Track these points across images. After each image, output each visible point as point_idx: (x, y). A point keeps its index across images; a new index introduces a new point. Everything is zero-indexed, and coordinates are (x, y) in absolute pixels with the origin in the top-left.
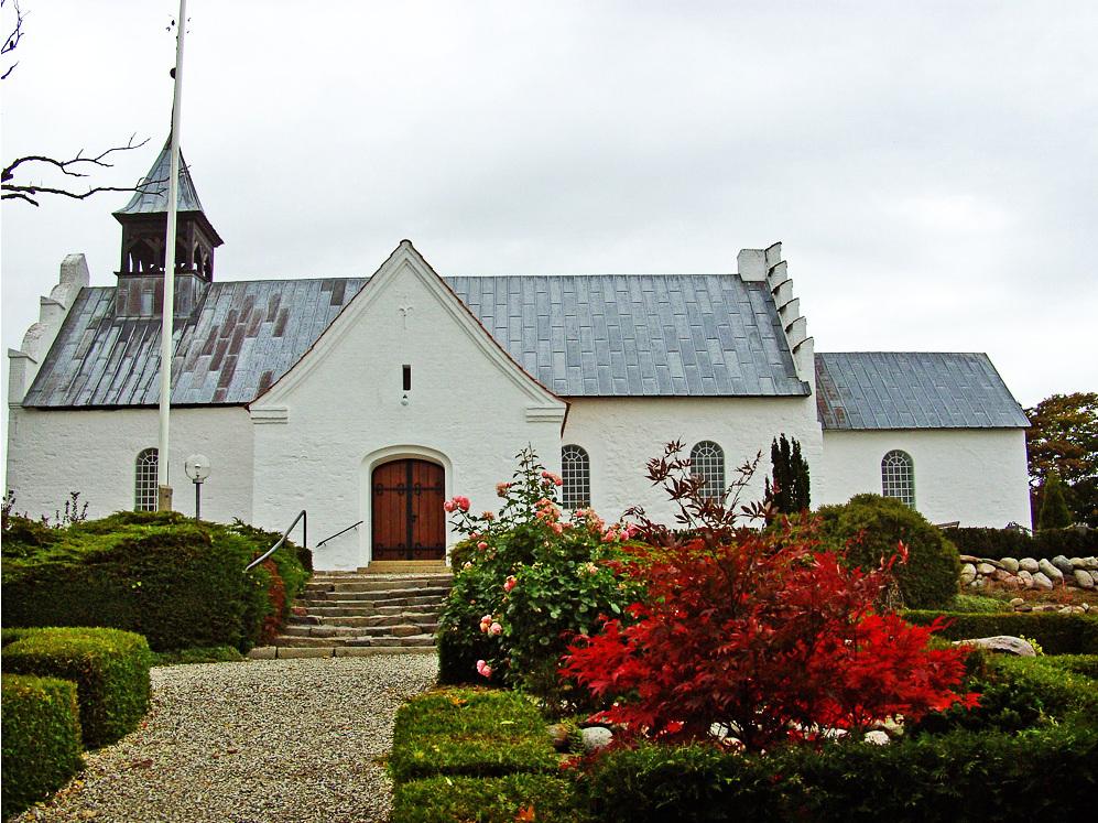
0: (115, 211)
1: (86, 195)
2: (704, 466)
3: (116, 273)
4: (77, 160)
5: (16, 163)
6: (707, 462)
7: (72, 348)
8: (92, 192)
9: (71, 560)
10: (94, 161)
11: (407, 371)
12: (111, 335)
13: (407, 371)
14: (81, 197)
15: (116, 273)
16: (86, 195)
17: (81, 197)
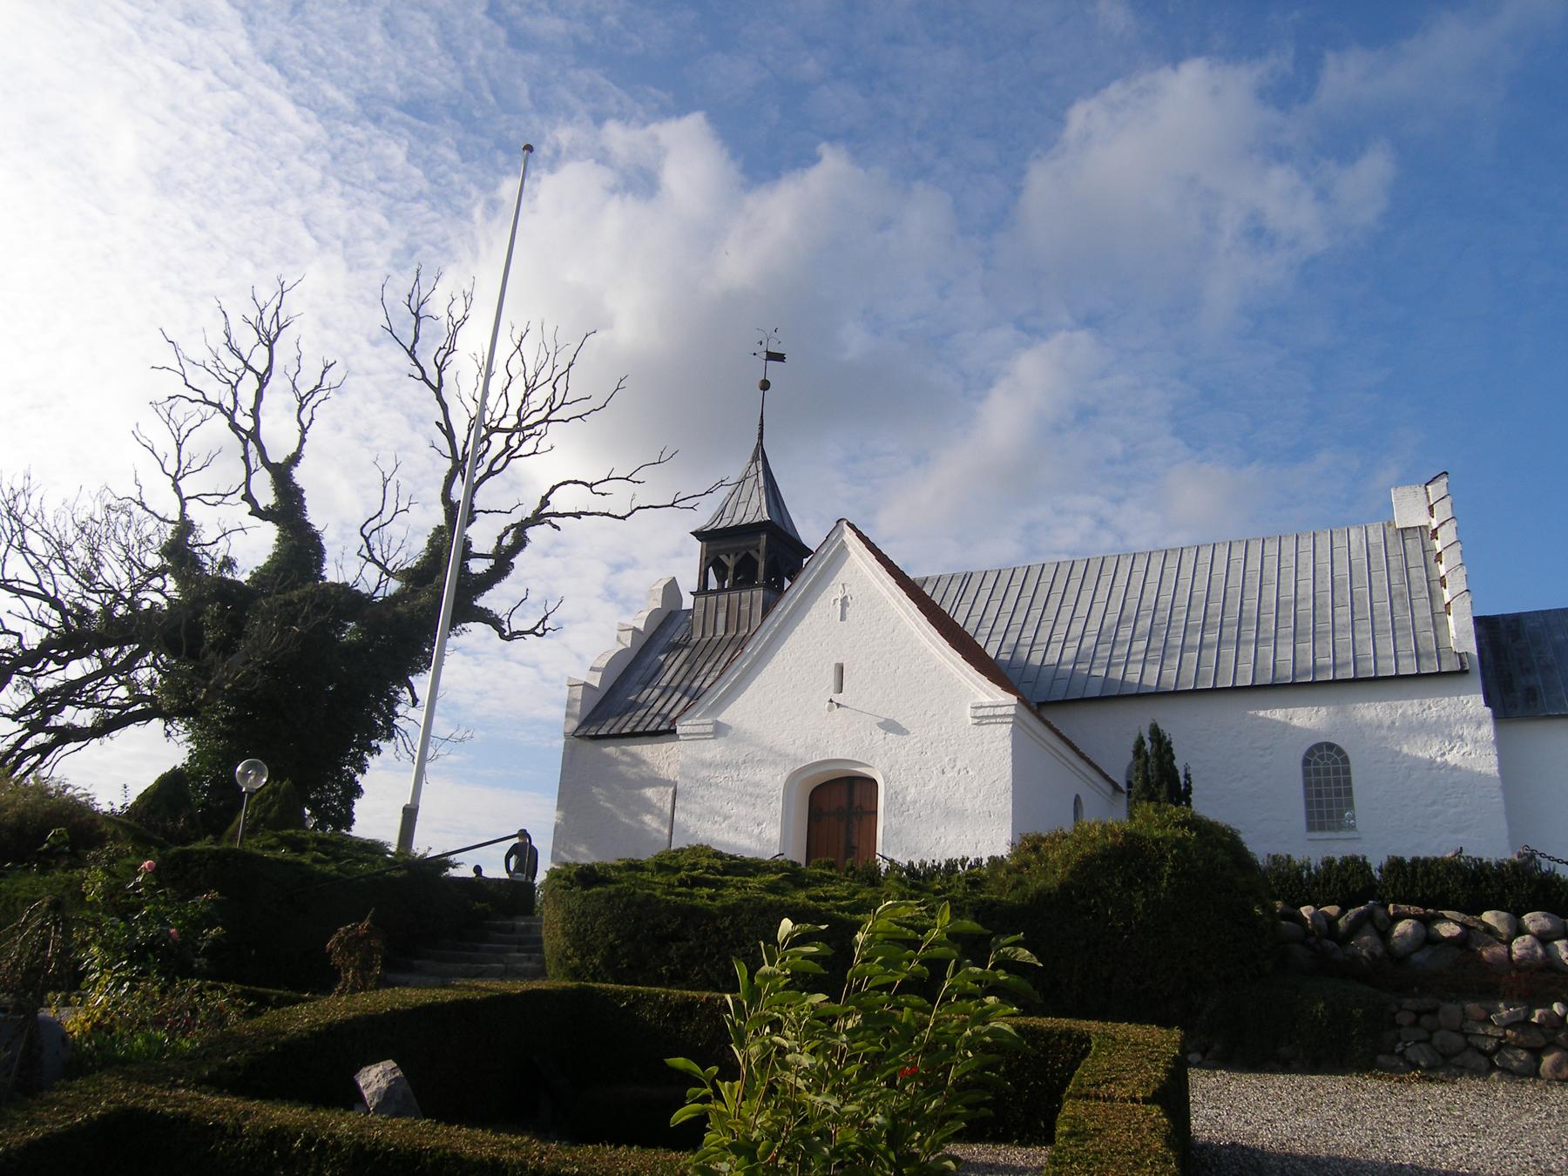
0: (693, 530)
1: (629, 515)
2: (1332, 777)
3: (692, 593)
4: (609, 479)
5: (554, 488)
6: (1327, 772)
7: (641, 672)
8: (633, 512)
9: (272, 805)
10: (627, 479)
11: (840, 669)
12: (680, 658)
13: (840, 669)
14: (623, 518)
15: (692, 593)
16: (629, 515)
17: (623, 518)
